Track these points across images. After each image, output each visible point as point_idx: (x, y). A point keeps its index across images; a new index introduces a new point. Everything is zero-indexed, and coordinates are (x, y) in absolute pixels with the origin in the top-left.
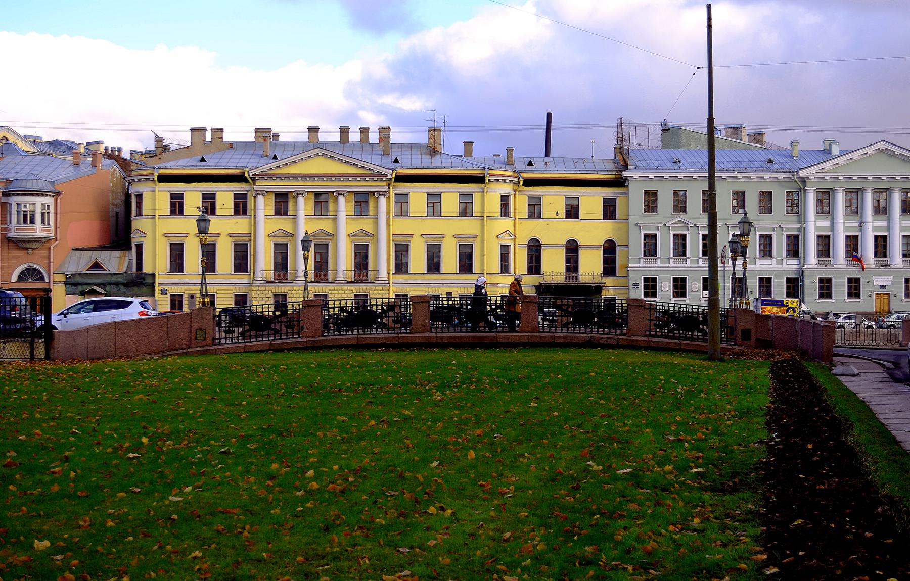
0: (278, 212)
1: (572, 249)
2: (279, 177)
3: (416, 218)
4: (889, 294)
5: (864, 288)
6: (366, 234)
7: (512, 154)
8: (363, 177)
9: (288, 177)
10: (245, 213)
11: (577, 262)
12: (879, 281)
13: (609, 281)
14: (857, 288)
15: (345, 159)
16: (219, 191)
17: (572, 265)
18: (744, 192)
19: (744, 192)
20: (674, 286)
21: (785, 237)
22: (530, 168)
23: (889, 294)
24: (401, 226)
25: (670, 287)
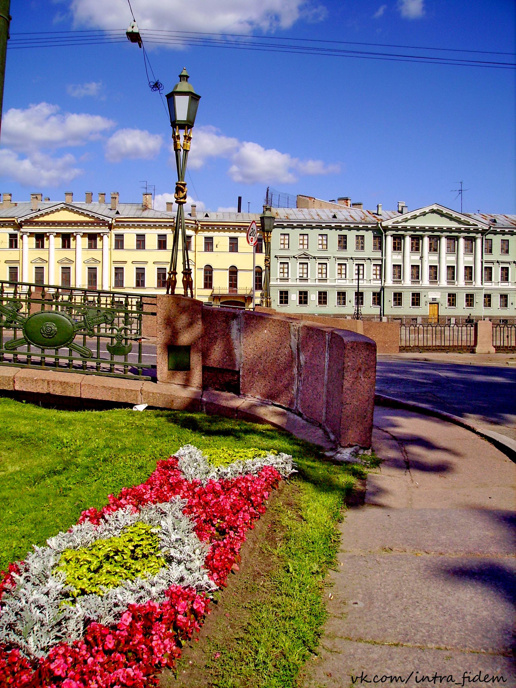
0: (37, 246)
1: (233, 272)
2: (37, 224)
3: (446, 258)
4: (438, 304)
5: (423, 300)
6: (95, 260)
7: (195, 209)
8: (87, 224)
9: (43, 223)
10: (16, 247)
11: (236, 281)
12: (432, 295)
13: (258, 293)
14: (418, 299)
15: (53, 209)
16: (126, 233)
17: (233, 283)
18: (346, 236)
19: (346, 236)
20: (319, 297)
21: (500, 268)
22: (207, 218)
23: (438, 304)
24: (119, 255)
25: (297, 299)
